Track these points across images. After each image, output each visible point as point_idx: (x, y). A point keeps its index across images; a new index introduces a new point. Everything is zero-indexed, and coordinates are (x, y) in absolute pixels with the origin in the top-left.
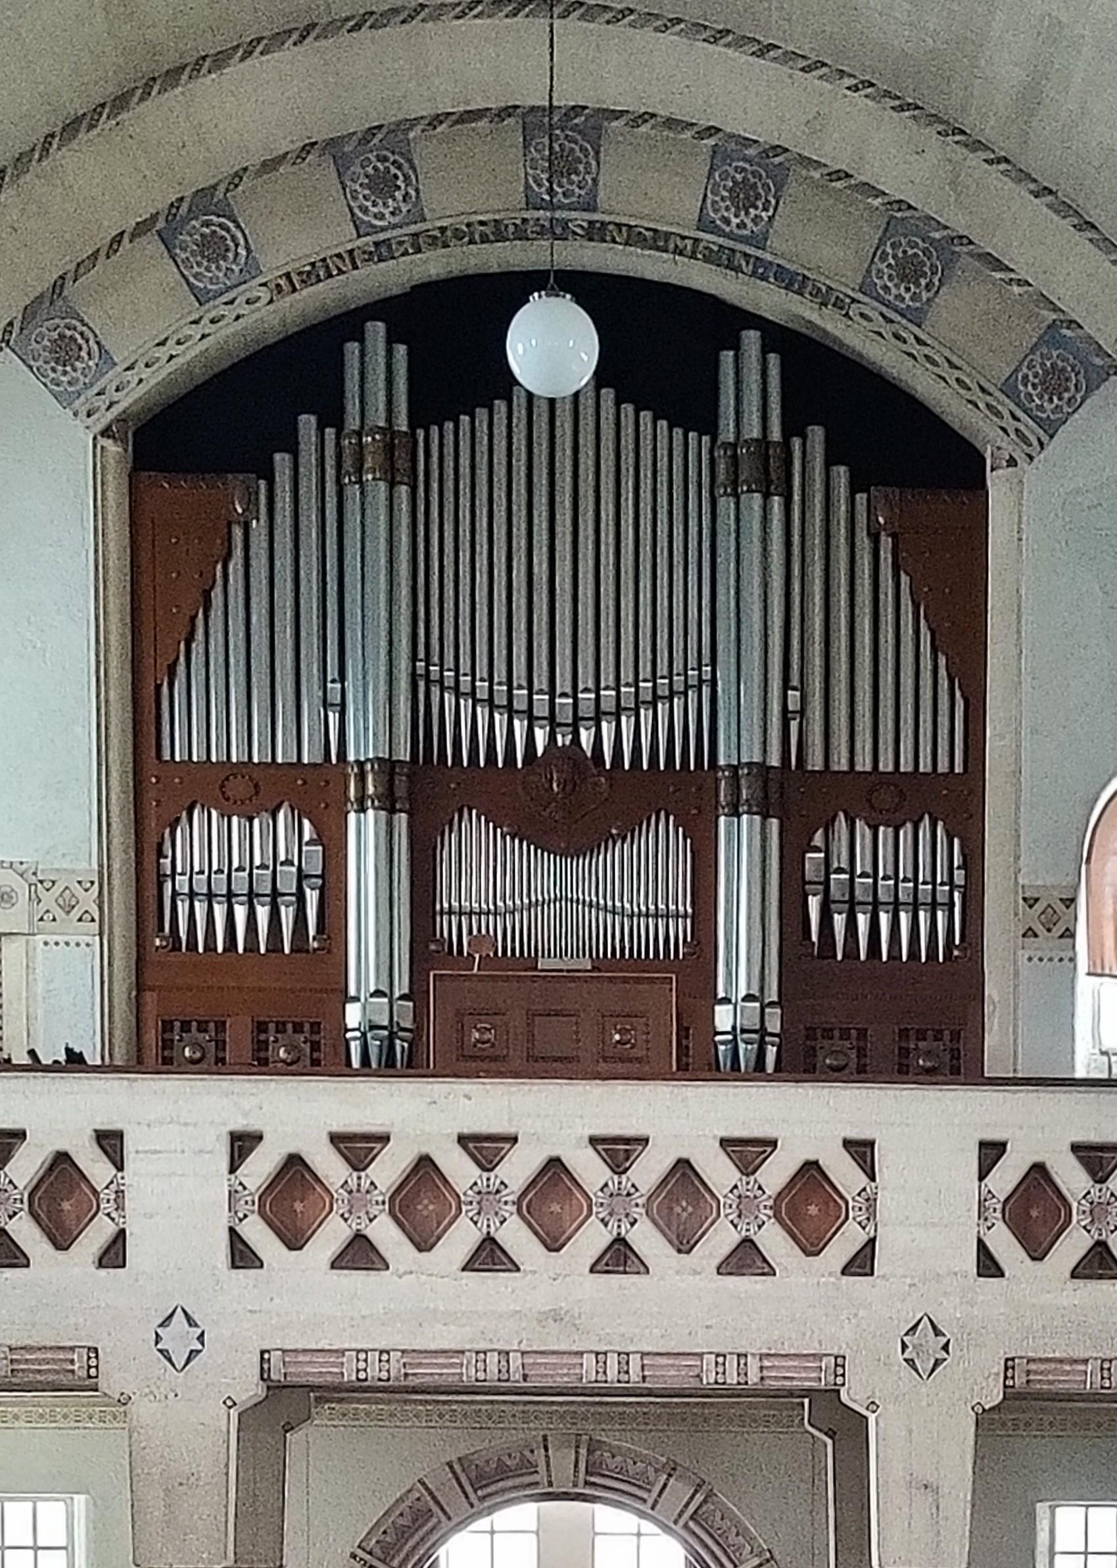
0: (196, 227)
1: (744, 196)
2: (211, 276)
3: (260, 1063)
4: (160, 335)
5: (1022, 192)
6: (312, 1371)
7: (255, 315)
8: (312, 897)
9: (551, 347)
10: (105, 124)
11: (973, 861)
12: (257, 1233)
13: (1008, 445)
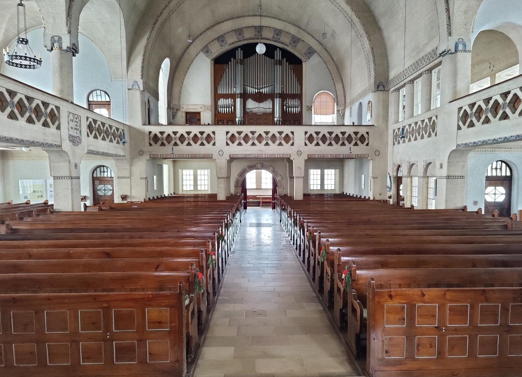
0: (221, 39)
1: (277, 35)
3: (227, 124)
4: (217, 50)
5: (306, 34)
6: (235, 156)
7: (227, 48)
8: (233, 107)
9: (261, 49)
12: (229, 142)
13: (305, 60)
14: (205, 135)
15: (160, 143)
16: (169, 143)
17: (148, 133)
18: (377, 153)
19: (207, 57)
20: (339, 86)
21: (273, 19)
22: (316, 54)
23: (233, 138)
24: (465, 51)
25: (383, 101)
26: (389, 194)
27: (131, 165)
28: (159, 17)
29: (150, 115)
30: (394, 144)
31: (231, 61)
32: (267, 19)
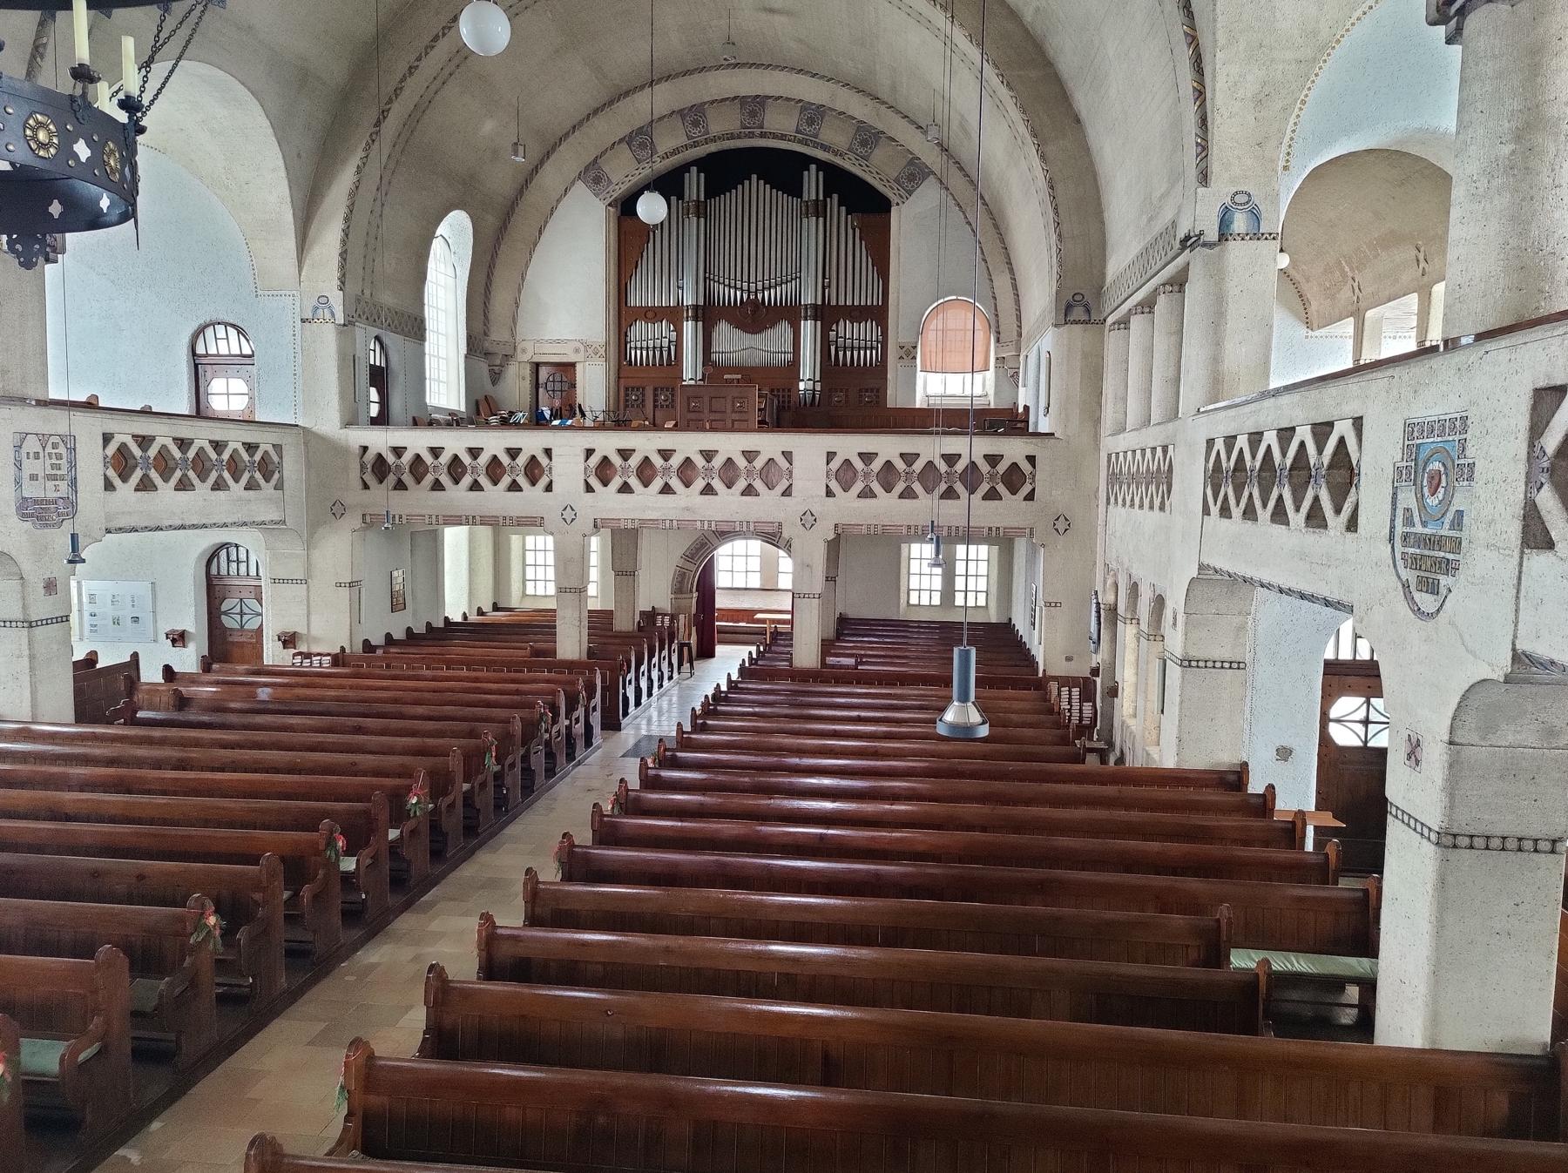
1: (811, 122)
2: (645, 153)
11: (885, 333)
14: (522, 460)
15: (391, 479)
17: (357, 451)
18: (1061, 525)
20: (1002, 282)
23: (604, 471)
24: (1257, 236)
25: (1085, 356)
27: (309, 545)
28: (390, 101)
29: (384, 385)
30: (1108, 503)
32: (776, 73)
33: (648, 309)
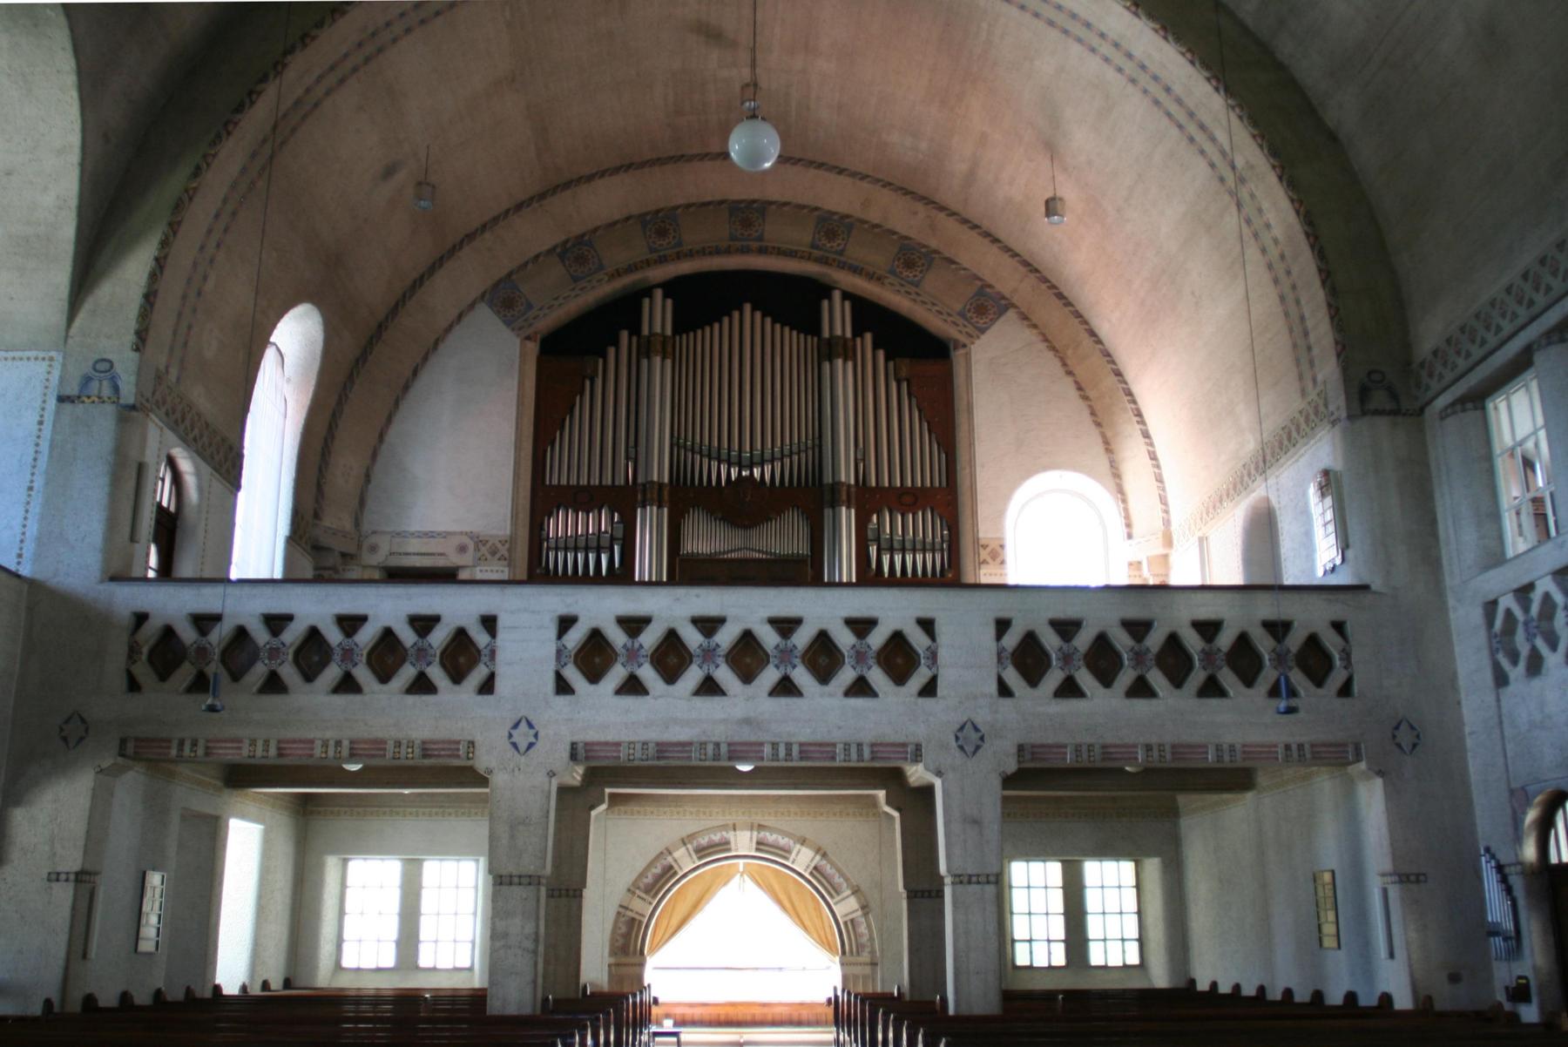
0: (576, 253)
1: (831, 234)
10: (535, 205)
12: (572, 674)
16: (236, 677)
19: (508, 323)
21: (812, 172)
22: (1011, 314)
23: (594, 656)
26: (1504, 974)
30: (1501, 679)
31: (616, 344)
33: (579, 489)
